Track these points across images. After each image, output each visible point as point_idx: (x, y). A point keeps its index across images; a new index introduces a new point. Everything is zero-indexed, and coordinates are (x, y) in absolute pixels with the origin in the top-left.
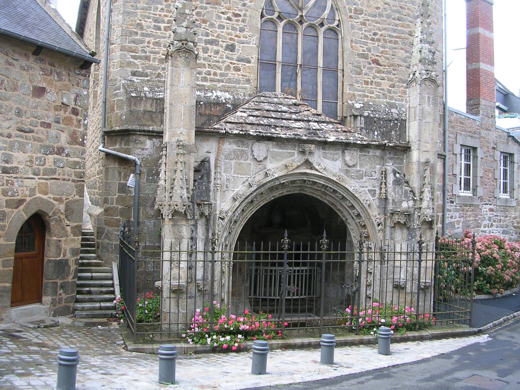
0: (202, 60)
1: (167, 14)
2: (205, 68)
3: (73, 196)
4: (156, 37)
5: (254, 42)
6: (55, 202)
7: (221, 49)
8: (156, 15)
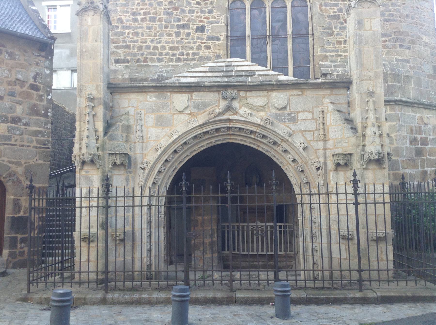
0: (175, 43)
1: (143, 7)
2: (179, 50)
3: (35, 160)
4: (134, 28)
5: (223, 21)
6: (10, 165)
7: (192, 32)
8: (134, 9)
